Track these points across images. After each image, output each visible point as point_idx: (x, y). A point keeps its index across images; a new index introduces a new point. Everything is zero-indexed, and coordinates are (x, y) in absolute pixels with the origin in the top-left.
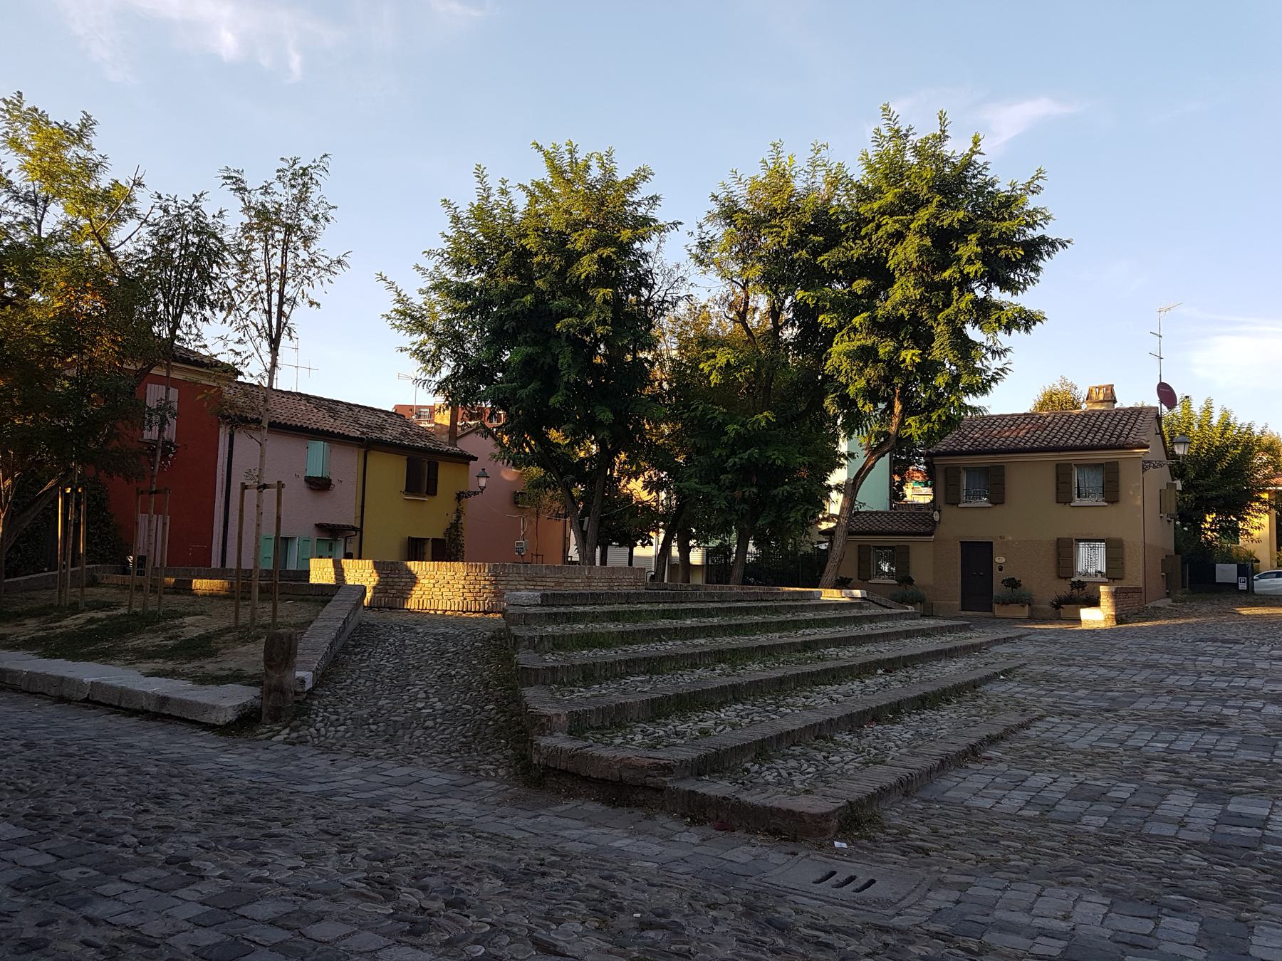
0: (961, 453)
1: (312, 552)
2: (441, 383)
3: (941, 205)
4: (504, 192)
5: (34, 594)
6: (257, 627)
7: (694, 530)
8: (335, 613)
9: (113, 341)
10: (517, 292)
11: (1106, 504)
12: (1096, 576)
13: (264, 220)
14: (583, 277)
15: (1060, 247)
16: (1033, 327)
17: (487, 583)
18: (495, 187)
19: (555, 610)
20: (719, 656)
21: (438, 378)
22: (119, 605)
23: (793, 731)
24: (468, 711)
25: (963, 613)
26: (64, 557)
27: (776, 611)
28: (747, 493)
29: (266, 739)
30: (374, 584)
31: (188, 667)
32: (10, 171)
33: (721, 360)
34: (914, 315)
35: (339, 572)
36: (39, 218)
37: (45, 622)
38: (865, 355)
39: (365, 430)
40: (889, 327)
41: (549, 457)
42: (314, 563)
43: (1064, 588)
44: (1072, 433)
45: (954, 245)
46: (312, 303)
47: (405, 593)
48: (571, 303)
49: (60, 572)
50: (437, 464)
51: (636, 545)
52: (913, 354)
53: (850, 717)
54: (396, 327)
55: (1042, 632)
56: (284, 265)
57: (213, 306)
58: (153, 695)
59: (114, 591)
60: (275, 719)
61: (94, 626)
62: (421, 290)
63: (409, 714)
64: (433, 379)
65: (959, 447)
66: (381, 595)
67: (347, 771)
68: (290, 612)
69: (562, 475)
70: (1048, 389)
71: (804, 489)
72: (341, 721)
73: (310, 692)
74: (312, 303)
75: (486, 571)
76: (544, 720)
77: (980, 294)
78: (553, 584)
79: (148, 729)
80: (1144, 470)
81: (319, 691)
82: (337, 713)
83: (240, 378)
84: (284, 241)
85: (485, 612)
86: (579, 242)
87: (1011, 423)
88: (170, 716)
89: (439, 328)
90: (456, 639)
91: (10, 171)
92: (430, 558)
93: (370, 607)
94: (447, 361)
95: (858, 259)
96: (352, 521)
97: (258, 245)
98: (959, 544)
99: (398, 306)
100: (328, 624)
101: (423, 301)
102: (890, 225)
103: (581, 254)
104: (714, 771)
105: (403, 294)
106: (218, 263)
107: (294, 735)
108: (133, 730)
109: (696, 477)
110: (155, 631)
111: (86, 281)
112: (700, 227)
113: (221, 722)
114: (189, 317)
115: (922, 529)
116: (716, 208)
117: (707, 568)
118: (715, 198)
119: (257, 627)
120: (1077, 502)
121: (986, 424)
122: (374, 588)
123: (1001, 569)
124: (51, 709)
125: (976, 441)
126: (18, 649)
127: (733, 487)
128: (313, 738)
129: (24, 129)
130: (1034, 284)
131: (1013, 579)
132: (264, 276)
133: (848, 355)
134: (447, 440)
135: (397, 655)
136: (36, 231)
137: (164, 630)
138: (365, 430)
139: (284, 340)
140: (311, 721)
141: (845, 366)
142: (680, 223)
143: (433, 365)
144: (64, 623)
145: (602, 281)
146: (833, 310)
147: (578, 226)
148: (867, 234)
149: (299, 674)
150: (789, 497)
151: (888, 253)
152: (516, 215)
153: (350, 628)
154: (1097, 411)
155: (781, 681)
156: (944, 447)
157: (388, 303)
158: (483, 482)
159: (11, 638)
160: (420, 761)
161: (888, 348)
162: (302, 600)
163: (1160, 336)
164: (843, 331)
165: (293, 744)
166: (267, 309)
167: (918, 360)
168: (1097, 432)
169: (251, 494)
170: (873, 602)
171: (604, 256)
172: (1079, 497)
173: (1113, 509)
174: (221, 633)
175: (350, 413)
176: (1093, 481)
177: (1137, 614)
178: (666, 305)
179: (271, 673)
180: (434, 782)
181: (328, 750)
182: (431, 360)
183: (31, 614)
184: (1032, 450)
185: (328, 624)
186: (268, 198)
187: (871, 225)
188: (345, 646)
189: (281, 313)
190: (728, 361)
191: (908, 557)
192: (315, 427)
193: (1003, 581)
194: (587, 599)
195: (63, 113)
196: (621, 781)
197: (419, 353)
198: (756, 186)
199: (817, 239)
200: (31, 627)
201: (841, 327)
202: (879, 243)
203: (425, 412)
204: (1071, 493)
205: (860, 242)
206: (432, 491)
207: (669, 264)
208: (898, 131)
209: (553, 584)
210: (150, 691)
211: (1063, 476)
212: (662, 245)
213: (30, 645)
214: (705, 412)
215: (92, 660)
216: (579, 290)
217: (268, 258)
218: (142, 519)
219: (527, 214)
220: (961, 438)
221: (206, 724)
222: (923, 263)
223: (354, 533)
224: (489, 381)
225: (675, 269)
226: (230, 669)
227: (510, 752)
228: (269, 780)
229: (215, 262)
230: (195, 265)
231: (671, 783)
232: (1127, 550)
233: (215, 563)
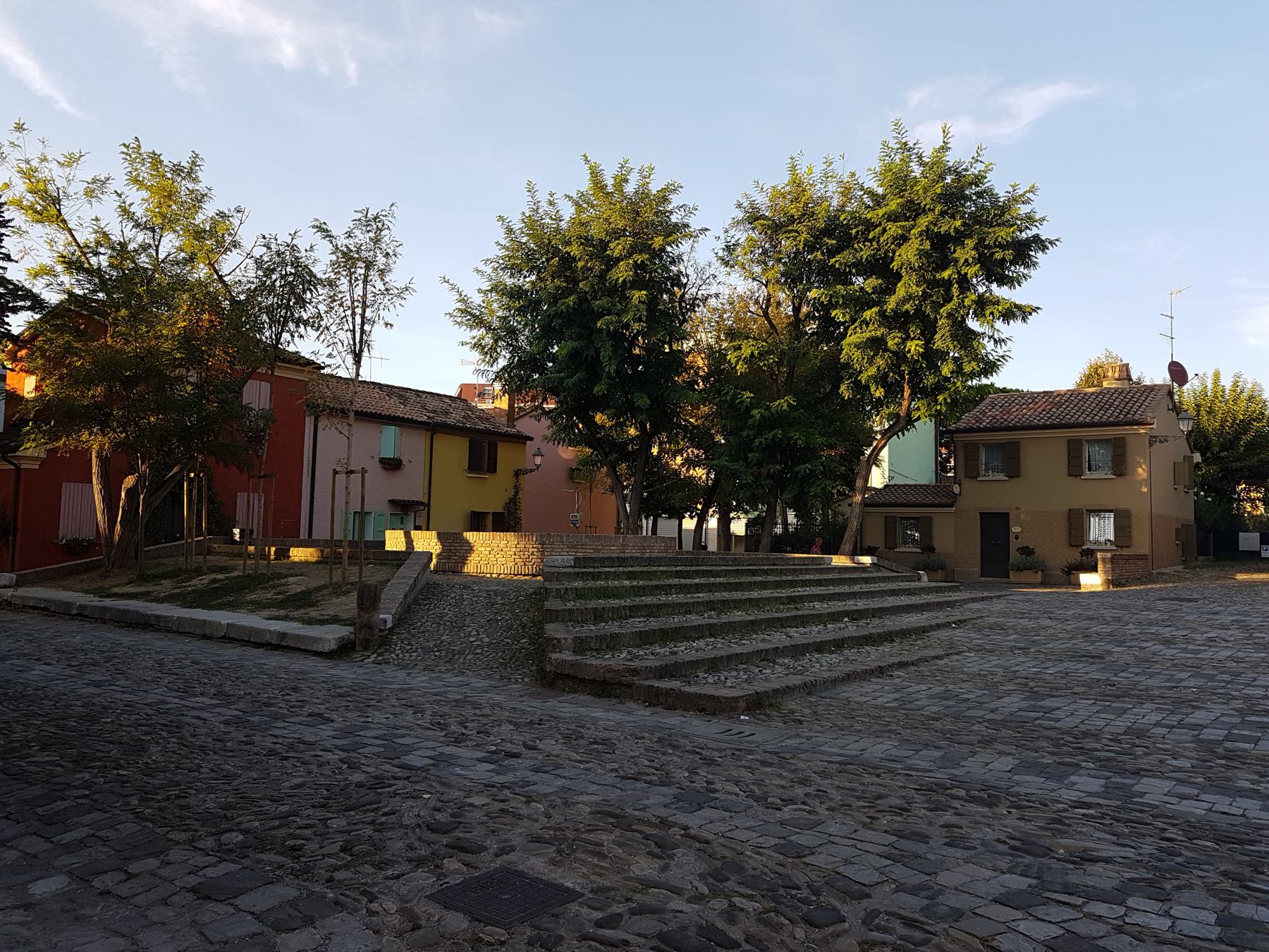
0: (979, 430)
1: (386, 524)
2: (498, 373)
3: (943, 213)
4: (551, 203)
5: (162, 560)
6: (347, 584)
7: (735, 503)
8: (407, 574)
9: (226, 353)
10: (566, 293)
11: (1114, 477)
12: (1106, 544)
13: (348, 260)
14: (620, 281)
15: (1049, 246)
16: (1029, 317)
17: (534, 550)
18: (543, 197)
19: (584, 570)
20: (711, 605)
21: (495, 368)
22: (233, 569)
23: (741, 653)
24: (508, 643)
25: (983, 579)
26: (190, 530)
27: (781, 572)
28: (772, 470)
29: (360, 661)
30: (438, 551)
31: (296, 614)
32: (132, 204)
33: (746, 352)
34: (918, 310)
35: (409, 541)
36: (157, 243)
37: (178, 582)
38: (876, 345)
39: (432, 415)
40: (898, 321)
41: (592, 437)
42: (388, 533)
43: (1074, 556)
44: (1084, 410)
45: (952, 248)
46: (387, 324)
47: (463, 560)
48: (611, 303)
49: (186, 542)
50: (496, 445)
51: (685, 517)
52: (917, 345)
53: (795, 647)
54: (458, 323)
55: (1037, 594)
56: (365, 295)
57: (306, 323)
58: (275, 631)
59: (225, 558)
60: (366, 648)
61: (217, 585)
62: (480, 289)
63: (464, 645)
64: (491, 369)
65: (978, 424)
66: (446, 561)
67: (419, 679)
68: (372, 575)
69: (607, 454)
70: (1093, 362)
71: (824, 467)
72: (414, 649)
73: (391, 630)
74: (387, 324)
75: (534, 539)
76: (556, 642)
77: (981, 289)
78: (592, 551)
79: (275, 655)
80: (1151, 445)
81: (397, 630)
82: (410, 644)
83: (325, 371)
84: (364, 275)
85: (533, 575)
86: (616, 248)
87: (1030, 401)
88: (288, 647)
89: (496, 324)
90: (504, 595)
91: (132, 204)
92: (491, 529)
93: (436, 571)
94: (504, 353)
95: (867, 259)
96: (418, 495)
97: (344, 281)
98: (978, 517)
99: (459, 305)
100: (403, 581)
101: (481, 299)
102: (893, 229)
103: (618, 260)
104: (672, 676)
105: (464, 294)
106: (311, 291)
107: (380, 658)
108: (263, 656)
109: (726, 455)
110: (267, 589)
111: (204, 304)
112: (726, 231)
113: (327, 649)
114: (289, 335)
115: (944, 500)
116: (740, 215)
117: (747, 540)
118: (739, 206)
119: (347, 584)
120: (1088, 475)
121: (1006, 402)
122: (438, 555)
123: (1017, 538)
124: (199, 643)
125: (994, 418)
126: (162, 602)
127: (759, 465)
128: (394, 660)
129: (143, 168)
130: (1026, 279)
131: (1027, 547)
132: (349, 303)
133: (858, 346)
134: (505, 422)
135: (456, 605)
136: (154, 254)
137: (273, 587)
138: (432, 415)
139: (365, 353)
140: (392, 649)
141: (857, 354)
142: (707, 230)
143: (491, 356)
144: (192, 583)
145: (637, 283)
146: (845, 305)
147: (617, 234)
148: (875, 237)
149: (381, 616)
150: (812, 474)
151: (894, 253)
152: (563, 222)
153: (419, 586)
154: (1111, 388)
155: (753, 623)
156: (965, 425)
157: (453, 304)
158: (538, 460)
159: (154, 594)
160: (471, 673)
161: (897, 339)
162: (381, 564)
163: (1172, 318)
164: (856, 324)
165: (379, 664)
166: (351, 328)
167: (921, 350)
168: (1108, 409)
169: (341, 478)
170: (884, 567)
171: (639, 262)
172: (1089, 470)
173: (1121, 481)
174: (319, 589)
175: (418, 399)
176: (1101, 454)
177: (1139, 579)
178: (697, 302)
179: (362, 613)
180: (479, 685)
181: (405, 667)
182: (490, 353)
183: (166, 576)
184: (1045, 427)
185: (403, 581)
186: (351, 241)
187: (878, 228)
188: (416, 600)
189: (363, 332)
190: (752, 352)
191: (931, 527)
192: (387, 414)
193: (1018, 549)
194: (614, 562)
195: (173, 155)
196: (605, 681)
197: (478, 346)
198: (778, 194)
199: (830, 242)
200: (167, 586)
201: (853, 321)
202: (886, 244)
203: (489, 390)
204: (1081, 466)
205: (869, 244)
206: (492, 469)
207: (702, 263)
208: (906, 144)
209: (592, 551)
210: (272, 629)
211: (1074, 450)
212: (695, 245)
213: (170, 599)
214: (734, 397)
215: (222, 609)
216: (619, 291)
217: (351, 291)
218: (241, 498)
219: (573, 222)
220: (981, 416)
221: (315, 651)
222: (923, 264)
223: (422, 508)
224: (542, 370)
225: (707, 267)
226: (328, 615)
227: (534, 668)
228: (365, 682)
229: (308, 289)
230: (292, 292)
231: (637, 680)
232: (1133, 519)
233: (303, 534)
